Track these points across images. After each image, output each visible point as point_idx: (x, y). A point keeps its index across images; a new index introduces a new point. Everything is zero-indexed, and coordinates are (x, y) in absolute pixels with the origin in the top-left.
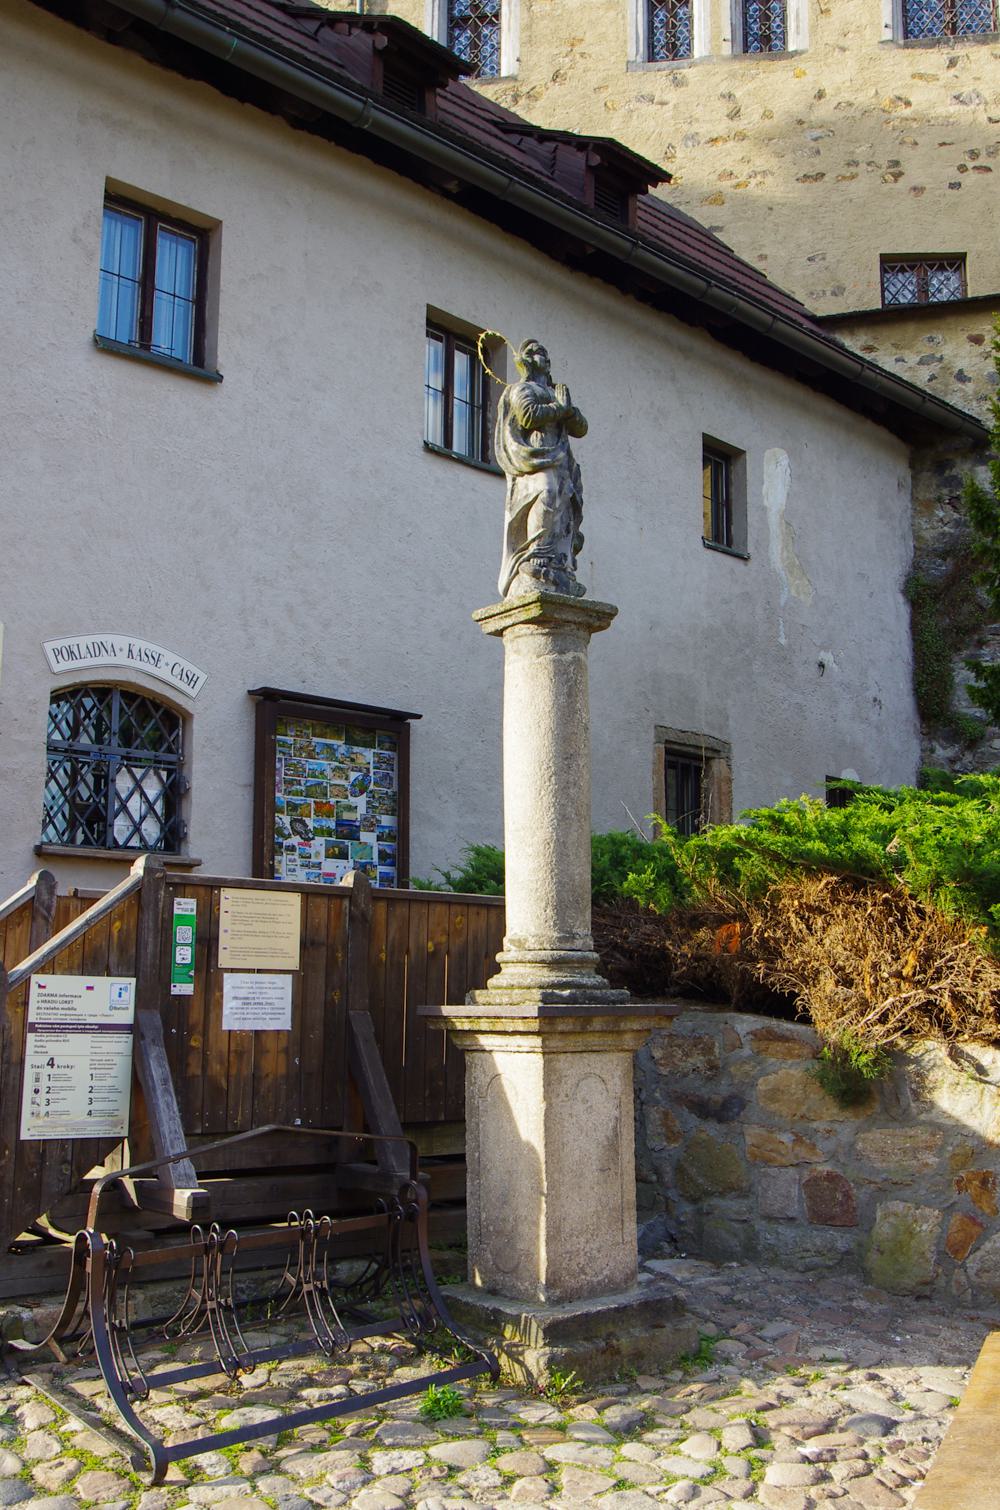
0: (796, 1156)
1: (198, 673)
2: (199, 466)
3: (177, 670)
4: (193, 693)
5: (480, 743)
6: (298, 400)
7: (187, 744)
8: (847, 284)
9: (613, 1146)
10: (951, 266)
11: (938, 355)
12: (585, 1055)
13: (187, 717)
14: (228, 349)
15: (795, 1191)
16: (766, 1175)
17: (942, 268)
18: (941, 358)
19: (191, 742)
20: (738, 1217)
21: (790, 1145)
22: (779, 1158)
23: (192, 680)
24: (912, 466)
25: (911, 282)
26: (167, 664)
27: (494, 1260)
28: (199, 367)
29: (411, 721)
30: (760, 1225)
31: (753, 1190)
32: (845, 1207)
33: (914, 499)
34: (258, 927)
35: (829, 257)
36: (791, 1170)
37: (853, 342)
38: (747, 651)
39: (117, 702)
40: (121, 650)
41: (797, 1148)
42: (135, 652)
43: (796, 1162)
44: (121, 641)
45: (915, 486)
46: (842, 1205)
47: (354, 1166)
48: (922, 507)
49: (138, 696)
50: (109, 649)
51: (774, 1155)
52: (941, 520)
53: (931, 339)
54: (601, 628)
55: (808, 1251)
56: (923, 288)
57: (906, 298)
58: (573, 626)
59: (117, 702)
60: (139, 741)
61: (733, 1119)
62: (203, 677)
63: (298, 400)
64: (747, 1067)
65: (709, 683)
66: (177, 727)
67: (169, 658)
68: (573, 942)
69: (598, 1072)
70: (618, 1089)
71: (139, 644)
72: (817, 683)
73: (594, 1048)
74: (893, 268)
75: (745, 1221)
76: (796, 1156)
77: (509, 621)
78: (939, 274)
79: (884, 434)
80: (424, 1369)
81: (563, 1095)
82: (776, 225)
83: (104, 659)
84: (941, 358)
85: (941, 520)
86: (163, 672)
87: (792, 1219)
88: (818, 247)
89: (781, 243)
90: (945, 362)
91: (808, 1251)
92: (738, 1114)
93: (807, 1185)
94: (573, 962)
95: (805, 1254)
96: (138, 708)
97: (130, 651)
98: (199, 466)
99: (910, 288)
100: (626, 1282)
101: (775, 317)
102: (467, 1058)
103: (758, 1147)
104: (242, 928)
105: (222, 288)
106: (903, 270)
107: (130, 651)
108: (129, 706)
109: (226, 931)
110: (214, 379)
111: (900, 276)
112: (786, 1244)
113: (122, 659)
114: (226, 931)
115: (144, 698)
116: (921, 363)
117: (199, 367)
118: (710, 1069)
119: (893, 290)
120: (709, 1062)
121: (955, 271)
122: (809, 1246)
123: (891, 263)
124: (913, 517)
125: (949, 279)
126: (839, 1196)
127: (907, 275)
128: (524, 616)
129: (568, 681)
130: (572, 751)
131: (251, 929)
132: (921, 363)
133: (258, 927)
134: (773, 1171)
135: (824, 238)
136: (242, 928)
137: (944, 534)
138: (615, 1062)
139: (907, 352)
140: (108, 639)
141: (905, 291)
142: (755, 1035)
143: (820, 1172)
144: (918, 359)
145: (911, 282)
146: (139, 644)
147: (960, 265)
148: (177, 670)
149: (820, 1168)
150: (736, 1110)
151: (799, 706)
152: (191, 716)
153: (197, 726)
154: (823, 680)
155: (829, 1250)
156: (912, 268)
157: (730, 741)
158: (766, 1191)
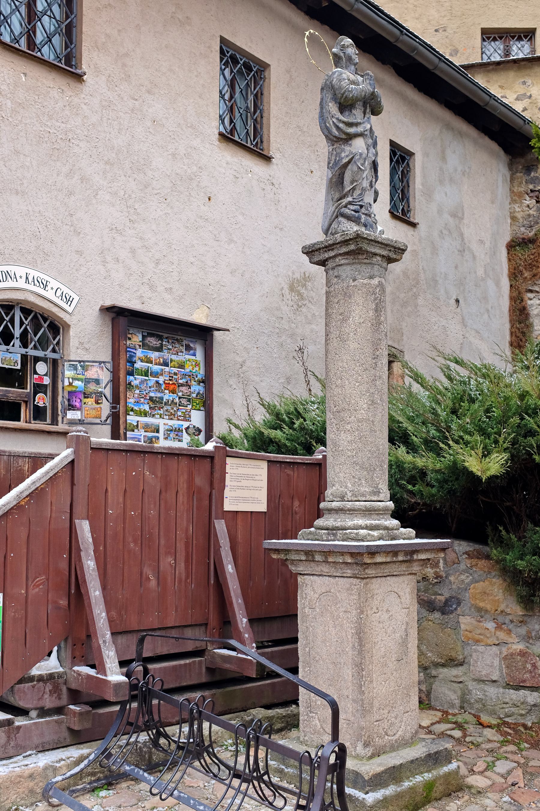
0: (498, 639)
1: (73, 295)
2: (71, 145)
3: (59, 293)
4: (70, 309)
5: (255, 349)
6: (136, 100)
7: (66, 346)
8: (459, 48)
9: (404, 642)
10: (526, 37)
11: (528, 94)
12: (388, 578)
13: (67, 327)
14: (89, 60)
15: (496, 662)
16: (476, 651)
17: (520, 39)
18: (530, 96)
19: (69, 345)
20: (456, 680)
21: (493, 630)
22: (485, 639)
23: (69, 301)
24: (510, 169)
25: (499, 49)
26: (52, 289)
27: (321, 725)
28: (68, 67)
29: (216, 333)
30: (471, 685)
31: (466, 661)
32: (533, 674)
33: (512, 191)
34: (244, 483)
35: (448, 30)
36: (494, 648)
37: (480, 80)
38: (415, 290)
39: (18, 315)
40: (21, 277)
41: (498, 633)
42: (30, 279)
43: (497, 642)
44: (21, 271)
45: (512, 180)
46: (531, 672)
47: (215, 651)
48: (516, 197)
49: (32, 311)
50: (13, 276)
51: (482, 637)
52: (528, 206)
53: (524, 83)
54: (396, 260)
55: (507, 703)
56: (507, 53)
57: (497, 58)
58: (379, 258)
59: (18, 315)
60: (33, 343)
61: (452, 612)
62: (76, 299)
63: (136, 100)
64: (463, 577)
65: (392, 311)
66: (59, 334)
67: (53, 284)
68: (378, 496)
69: (396, 590)
70: (408, 601)
71: (33, 273)
72: (455, 313)
73: (395, 573)
74: (488, 38)
75: (461, 682)
76: (498, 639)
77: (331, 254)
78: (517, 43)
79: (494, 146)
80: (152, 736)
81: (375, 608)
82: (415, 6)
83: (10, 284)
84: (530, 96)
85: (528, 206)
86: (49, 294)
87: (494, 681)
88: (442, 23)
89: (417, 19)
90: (533, 98)
91: (507, 703)
92: (456, 609)
93: (505, 658)
94: (380, 510)
95: (504, 706)
96: (32, 319)
97: (27, 278)
98: (71, 145)
99: (499, 52)
100: (412, 739)
101: (440, 59)
102: (299, 579)
103: (470, 632)
104: (235, 484)
105: (84, 12)
106: (495, 39)
107: (27, 278)
108: (26, 319)
109: (226, 498)
110: (79, 77)
111: (493, 43)
112: (491, 699)
113: (21, 284)
114: (226, 498)
115: (36, 313)
116: (517, 99)
117: (68, 67)
118: (436, 578)
119: (488, 53)
120: (436, 573)
121: (528, 41)
122: (507, 700)
123: (489, 35)
124: (510, 204)
125: (523, 47)
126: (529, 666)
127: (497, 43)
128: (344, 250)
129: (375, 299)
130: (378, 353)
131: (239, 484)
132: (517, 99)
133: (244, 483)
134: (481, 648)
135: (445, 16)
136: (235, 484)
137: (529, 215)
138: (406, 582)
139: (508, 91)
140: (12, 269)
141: (495, 52)
142: (469, 555)
143: (515, 650)
144: (515, 96)
145: (499, 49)
146: (33, 273)
147: (531, 37)
148: (59, 293)
149: (514, 647)
150: (454, 606)
151: (444, 327)
152: (69, 326)
153: (72, 332)
154: (459, 310)
155: (522, 703)
156: (501, 38)
157: (404, 350)
158: (476, 662)
